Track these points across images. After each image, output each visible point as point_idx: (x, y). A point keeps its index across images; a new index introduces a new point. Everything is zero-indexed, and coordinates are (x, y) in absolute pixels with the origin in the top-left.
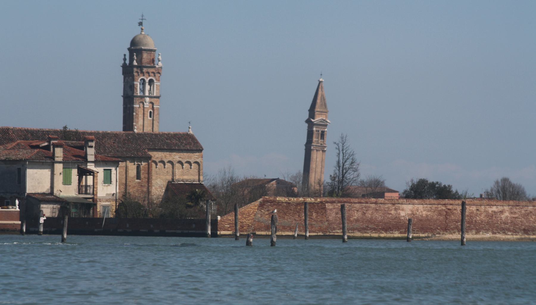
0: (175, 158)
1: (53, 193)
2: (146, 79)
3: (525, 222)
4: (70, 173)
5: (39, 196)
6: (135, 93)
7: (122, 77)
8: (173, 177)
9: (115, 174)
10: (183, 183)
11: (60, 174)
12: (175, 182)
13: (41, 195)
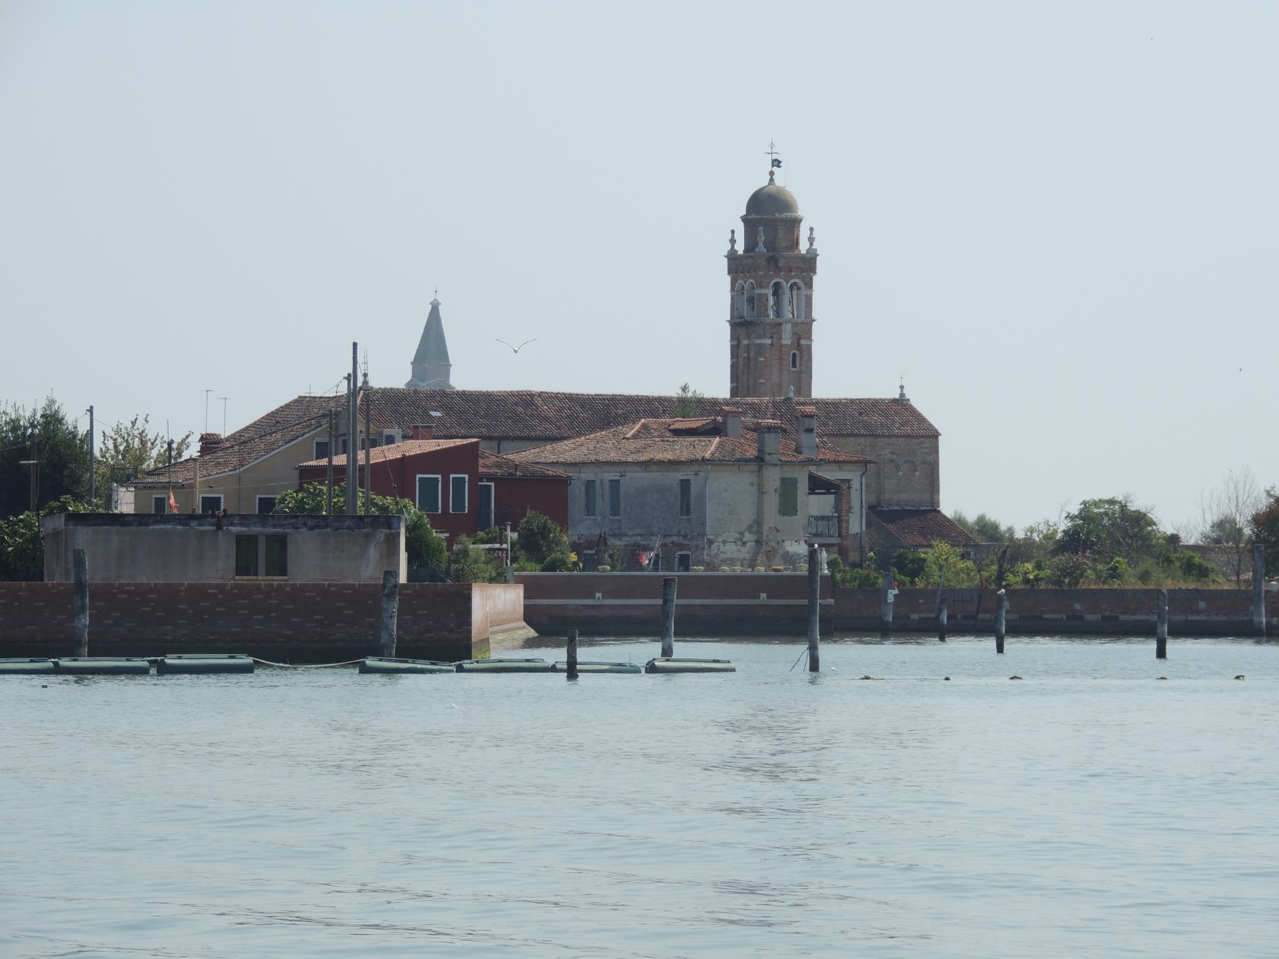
0: (882, 453)
2: (784, 283)
7: (727, 280)
9: (859, 491)
11: (776, 490)
12: (883, 507)
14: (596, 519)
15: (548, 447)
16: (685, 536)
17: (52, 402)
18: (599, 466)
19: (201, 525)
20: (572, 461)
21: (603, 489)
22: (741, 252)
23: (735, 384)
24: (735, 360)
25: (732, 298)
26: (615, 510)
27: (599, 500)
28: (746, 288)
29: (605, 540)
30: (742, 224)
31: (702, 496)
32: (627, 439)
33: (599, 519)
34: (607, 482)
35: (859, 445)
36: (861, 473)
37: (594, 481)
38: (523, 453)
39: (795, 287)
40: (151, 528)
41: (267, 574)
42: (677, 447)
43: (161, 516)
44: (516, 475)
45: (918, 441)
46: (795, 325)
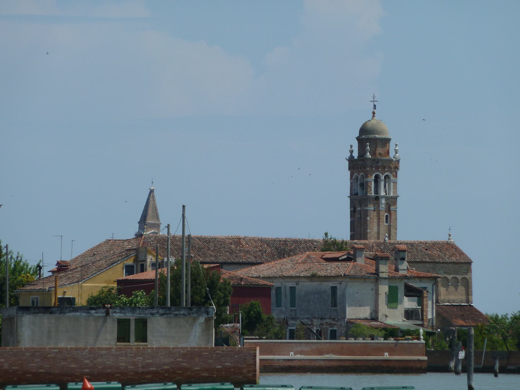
1: (378, 318)
2: (381, 175)
3: (16, 347)
4: (61, 295)
5: (361, 323)
6: (368, 193)
8: (438, 298)
10: (449, 304)
12: (440, 303)
13: (363, 321)
14: (281, 309)
15: (253, 268)
16: (334, 319)
17: (327, 232)
18: (283, 279)
19: (96, 313)
20: (268, 276)
21: (286, 292)
22: (356, 157)
23: (353, 233)
24: (353, 219)
25: (351, 183)
26: (293, 304)
27: (283, 298)
28: (359, 178)
29: (287, 321)
30: (357, 141)
31: (343, 296)
32: (299, 263)
33: (283, 309)
34: (288, 288)
35: (426, 268)
36: (433, 283)
37: (281, 287)
38: (239, 271)
39: (387, 177)
40: (67, 314)
41: (136, 341)
42: (329, 268)
43: (73, 307)
44: (241, 284)
45: (459, 265)
46: (387, 198)
